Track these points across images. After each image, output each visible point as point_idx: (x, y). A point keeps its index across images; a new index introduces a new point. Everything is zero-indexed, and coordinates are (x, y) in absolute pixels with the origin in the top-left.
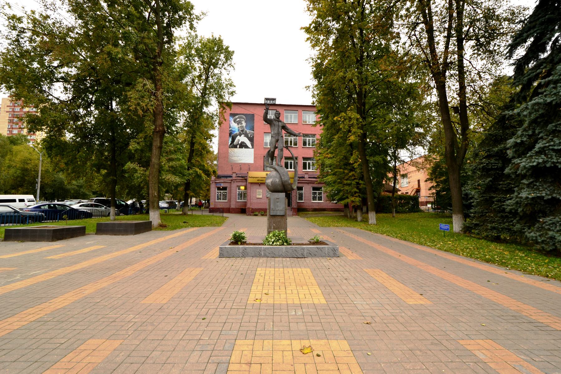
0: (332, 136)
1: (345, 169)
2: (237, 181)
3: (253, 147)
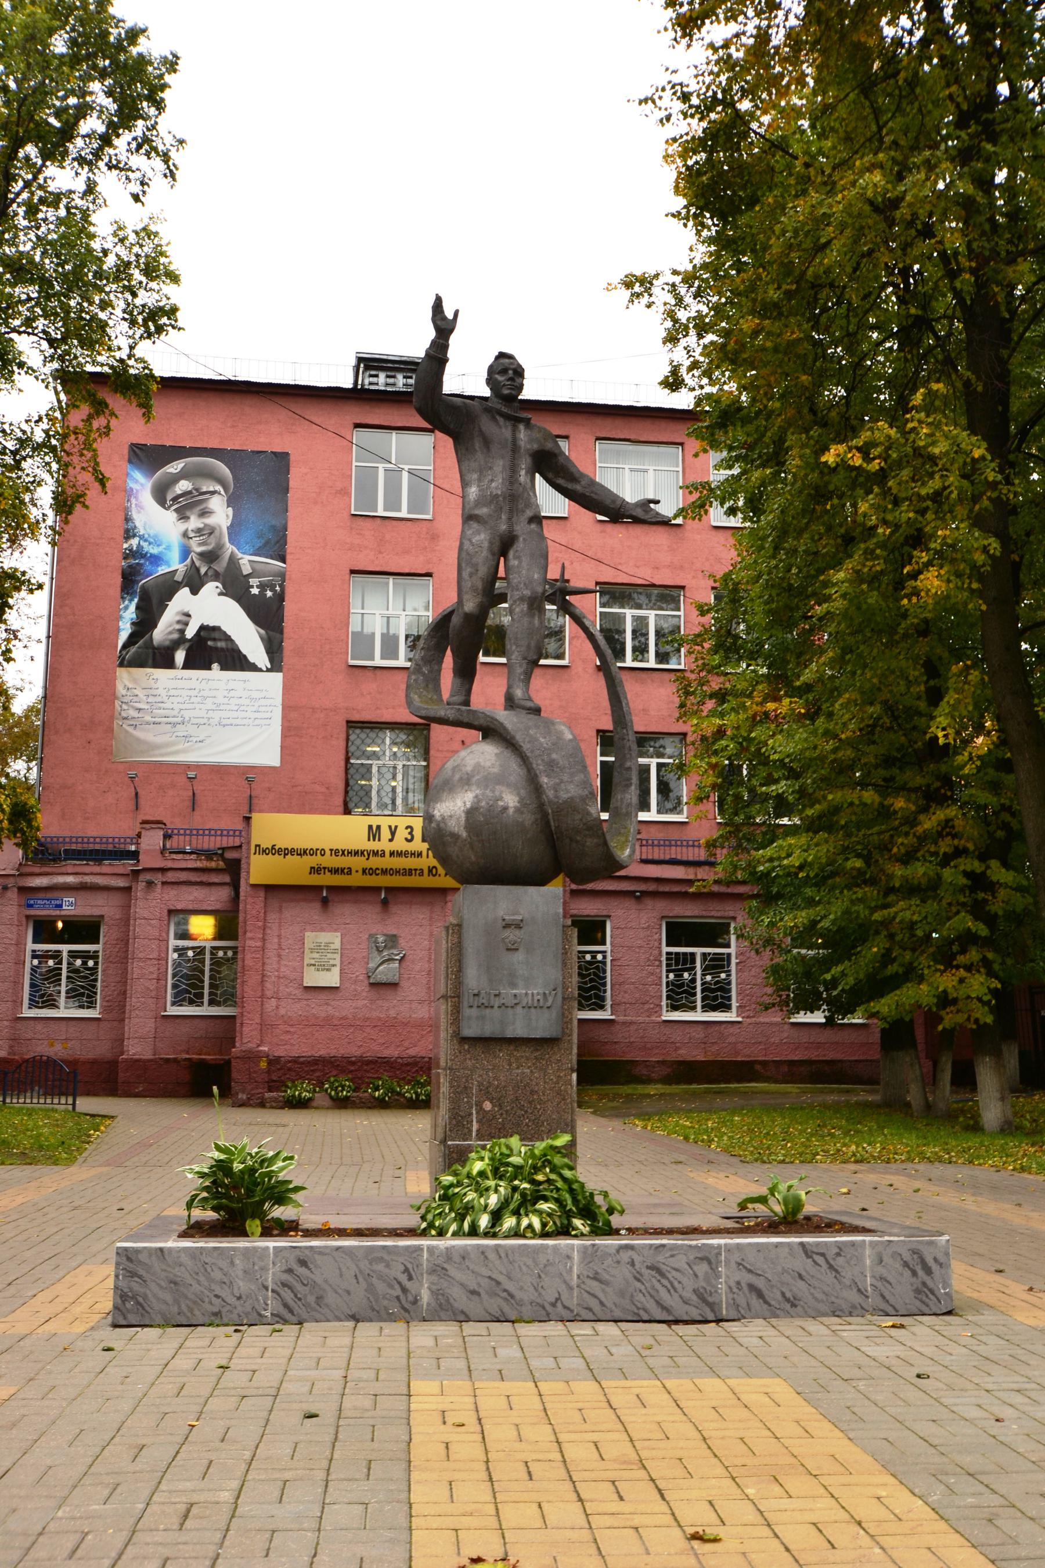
0: (821, 571)
1: (887, 787)
2: (170, 876)
3: (276, 666)
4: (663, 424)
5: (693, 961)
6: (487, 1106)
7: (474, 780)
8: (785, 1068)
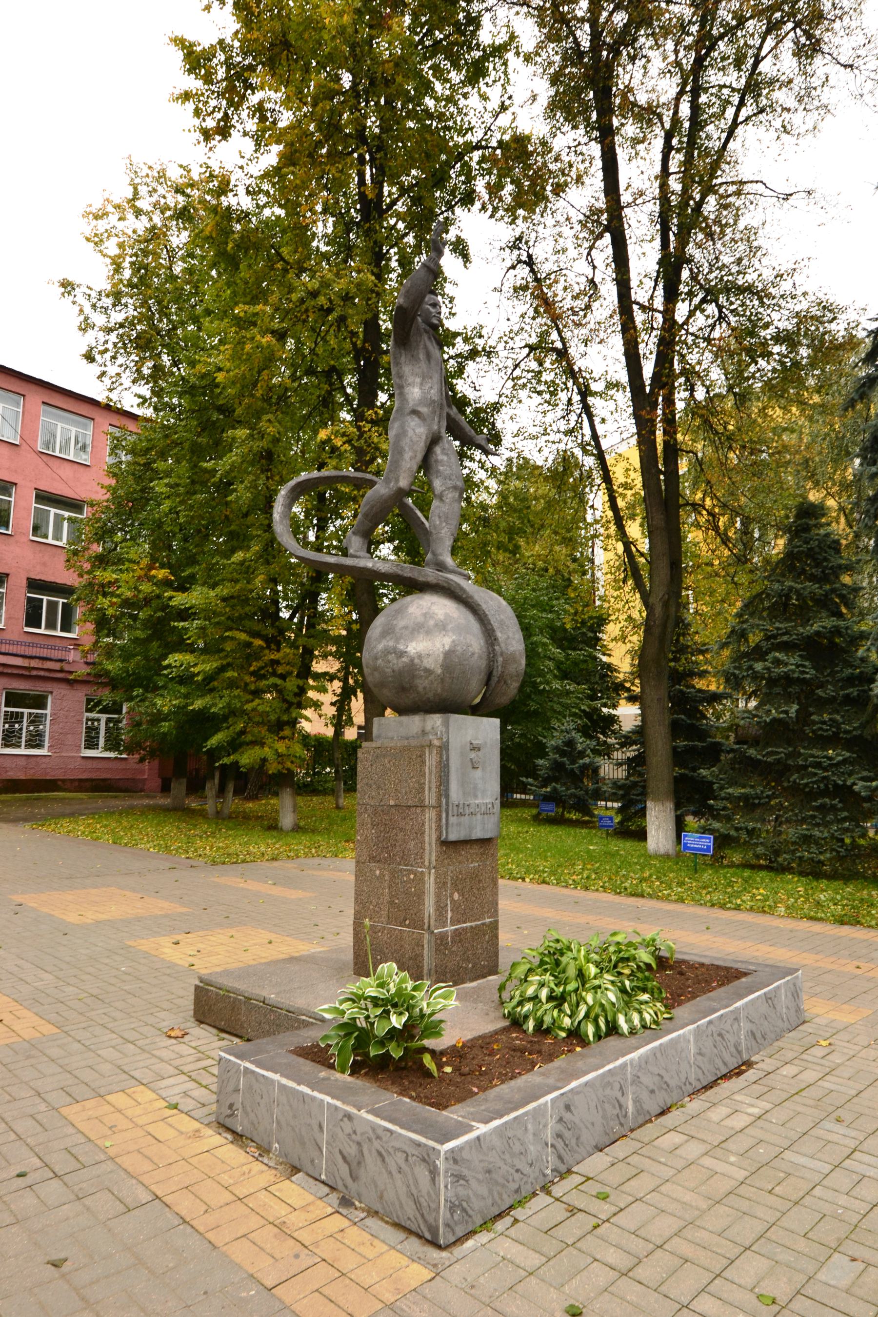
4: (13, 380)
5: (22, 717)
6: (456, 896)
7: (450, 627)
8: (77, 784)
